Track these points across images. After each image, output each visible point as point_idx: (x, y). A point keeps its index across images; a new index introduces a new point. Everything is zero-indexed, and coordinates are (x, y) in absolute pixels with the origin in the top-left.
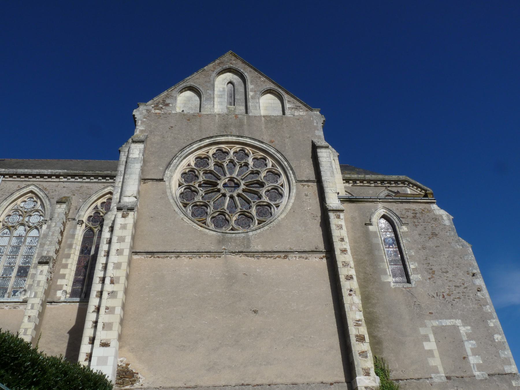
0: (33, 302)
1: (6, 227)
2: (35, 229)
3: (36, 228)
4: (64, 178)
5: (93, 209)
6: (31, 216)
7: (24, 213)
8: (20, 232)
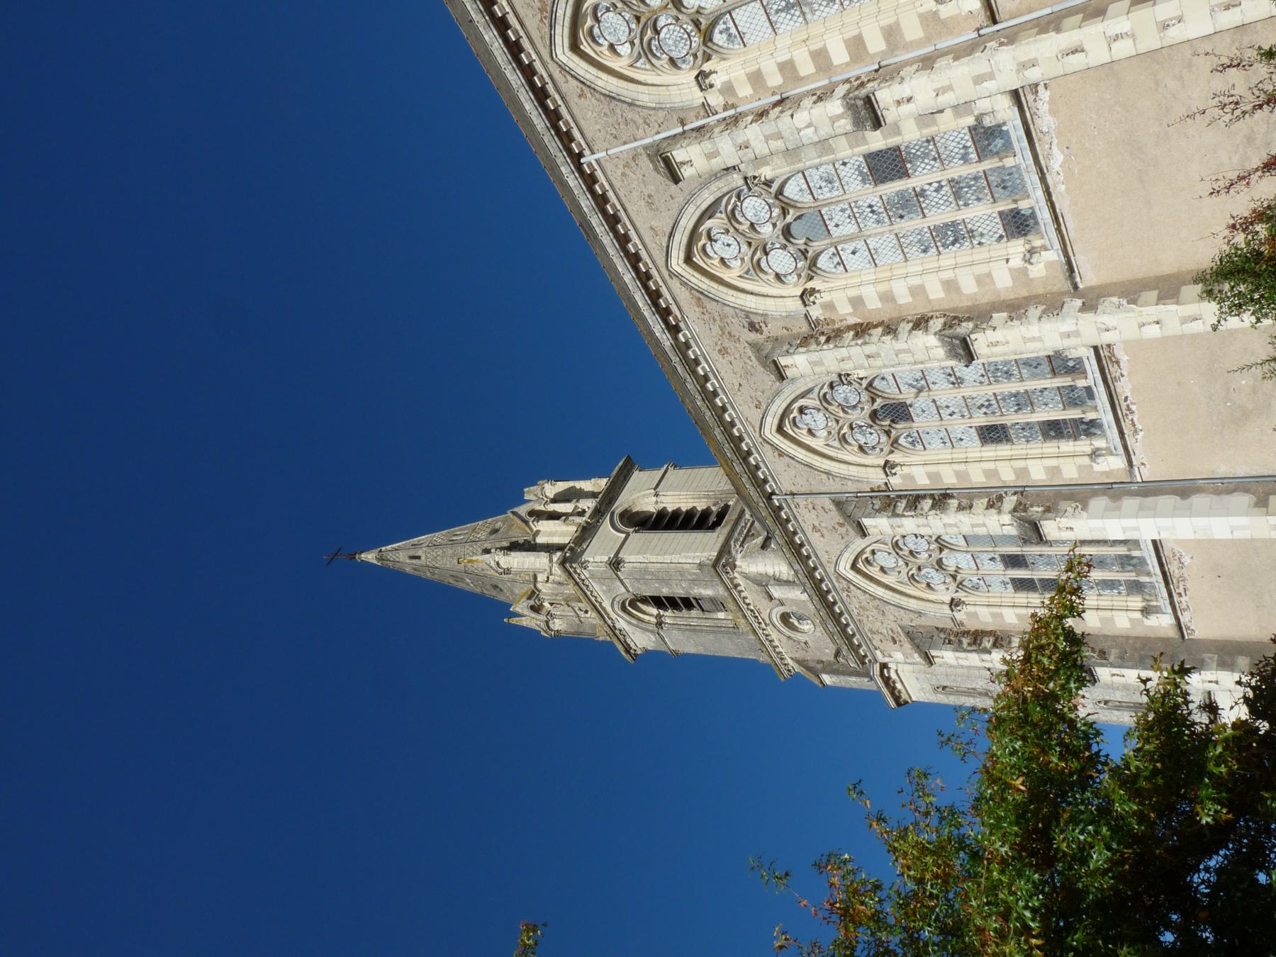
1: (870, 389)
2: (785, 194)
3: (780, 192)
7: (643, 20)
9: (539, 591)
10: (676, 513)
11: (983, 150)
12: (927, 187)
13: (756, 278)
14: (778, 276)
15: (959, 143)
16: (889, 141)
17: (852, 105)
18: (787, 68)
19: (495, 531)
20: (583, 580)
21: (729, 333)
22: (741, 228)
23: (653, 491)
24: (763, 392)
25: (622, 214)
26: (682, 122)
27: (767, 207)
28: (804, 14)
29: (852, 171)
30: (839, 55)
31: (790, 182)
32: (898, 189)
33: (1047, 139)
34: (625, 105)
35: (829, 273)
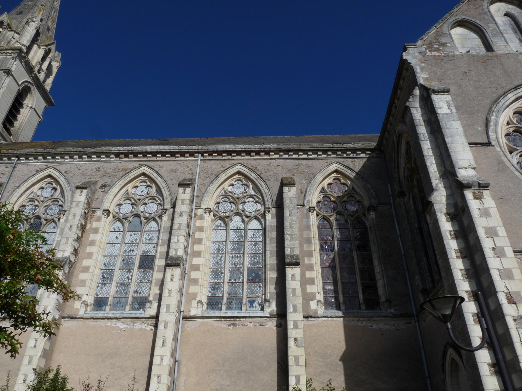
0: (295, 319)
1: (52, 221)
2: (152, 221)
3: (154, 219)
4: (275, 154)
5: (319, 193)
6: (244, 203)
7: (237, 200)
8: (236, 223)
9: (10, 31)
10: (18, 112)
11: (136, 299)
12: (131, 274)
13: (123, 197)
14: (120, 205)
15: (143, 291)
16: (157, 266)
17: (179, 259)
18: (199, 241)
19: (48, 29)
20: (6, 53)
21: (105, 175)
22: (147, 199)
23: (34, 107)
24: (72, 177)
25: (173, 159)
26: (197, 197)
27: (150, 212)
28: (214, 254)
29: (150, 249)
30: (196, 261)
31: (156, 225)
32: (136, 263)
33: (131, 324)
34: (212, 180)
35: (113, 225)
